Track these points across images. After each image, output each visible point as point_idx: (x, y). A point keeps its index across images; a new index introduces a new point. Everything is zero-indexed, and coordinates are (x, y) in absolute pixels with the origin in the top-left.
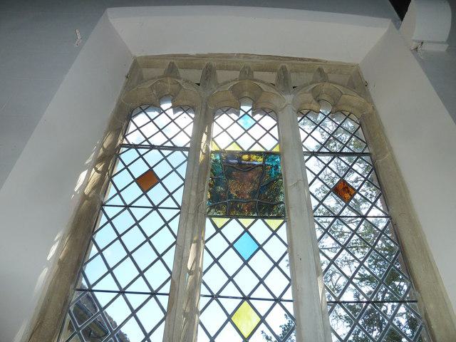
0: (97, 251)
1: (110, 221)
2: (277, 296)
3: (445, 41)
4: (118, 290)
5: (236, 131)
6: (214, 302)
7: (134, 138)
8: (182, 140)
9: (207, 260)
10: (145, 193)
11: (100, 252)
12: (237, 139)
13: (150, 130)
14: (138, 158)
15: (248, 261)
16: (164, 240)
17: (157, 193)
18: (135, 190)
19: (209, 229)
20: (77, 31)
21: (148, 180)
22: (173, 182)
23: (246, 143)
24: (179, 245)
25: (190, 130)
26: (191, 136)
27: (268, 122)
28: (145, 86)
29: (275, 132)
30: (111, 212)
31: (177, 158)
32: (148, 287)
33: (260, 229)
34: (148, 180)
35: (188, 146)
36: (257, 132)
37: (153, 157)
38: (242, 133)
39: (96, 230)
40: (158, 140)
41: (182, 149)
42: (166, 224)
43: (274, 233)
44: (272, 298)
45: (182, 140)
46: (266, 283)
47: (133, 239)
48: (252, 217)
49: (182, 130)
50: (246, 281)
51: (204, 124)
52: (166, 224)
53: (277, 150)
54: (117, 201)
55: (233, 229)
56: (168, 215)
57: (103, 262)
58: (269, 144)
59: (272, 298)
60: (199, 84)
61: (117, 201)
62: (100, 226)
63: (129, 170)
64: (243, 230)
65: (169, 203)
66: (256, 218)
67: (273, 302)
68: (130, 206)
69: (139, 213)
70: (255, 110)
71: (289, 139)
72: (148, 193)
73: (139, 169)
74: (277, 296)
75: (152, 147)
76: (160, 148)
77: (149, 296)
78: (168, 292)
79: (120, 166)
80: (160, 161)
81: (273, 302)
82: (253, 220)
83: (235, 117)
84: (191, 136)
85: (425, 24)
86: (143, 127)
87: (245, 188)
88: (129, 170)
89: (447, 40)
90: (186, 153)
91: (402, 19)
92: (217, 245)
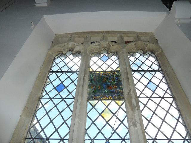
0: (37, 121)
1: (43, 106)
3: (190, 18)
4: (49, 140)
5: (100, 63)
7: (55, 69)
9: (69, 122)
10: (59, 93)
11: (139, 67)
12: (103, 63)
13: (61, 65)
14: (49, 92)
16: (67, 114)
17: (64, 93)
18: (55, 92)
19: (89, 107)
20: (32, 22)
21: (60, 88)
22: (72, 87)
23: (104, 67)
26: (79, 66)
27: (114, 58)
28: (60, 46)
29: (117, 62)
30: (43, 101)
33: (114, 105)
34: (60, 88)
35: (78, 70)
36: (109, 62)
37: (63, 77)
39: (36, 111)
40: (65, 69)
41: (76, 72)
42: (68, 106)
43: (120, 107)
46: (40, 123)
47: (53, 114)
49: (76, 64)
50: (107, 132)
54: (47, 97)
55: (100, 106)
57: (65, 135)
58: (115, 67)
59: (167, 138)
60: (82, 43)
61: (47, 97)
62: (39, 108)
64: (105, 107)
65: (70, 96)
68: (53, 98)
72: (60, 93)
73: (57, 83)
74: (123, 137)
75: (62, 72)
76: (65, 72)
78: (68, 138)
79: (54, 64)
83: (100, 57)
84: (79, 66)
85: (179, 10)
86: (59, 63)
87: (106, 86)
89: (190, 18)
90: (78, 73)
91: (170, 10)
92: (93, 115)
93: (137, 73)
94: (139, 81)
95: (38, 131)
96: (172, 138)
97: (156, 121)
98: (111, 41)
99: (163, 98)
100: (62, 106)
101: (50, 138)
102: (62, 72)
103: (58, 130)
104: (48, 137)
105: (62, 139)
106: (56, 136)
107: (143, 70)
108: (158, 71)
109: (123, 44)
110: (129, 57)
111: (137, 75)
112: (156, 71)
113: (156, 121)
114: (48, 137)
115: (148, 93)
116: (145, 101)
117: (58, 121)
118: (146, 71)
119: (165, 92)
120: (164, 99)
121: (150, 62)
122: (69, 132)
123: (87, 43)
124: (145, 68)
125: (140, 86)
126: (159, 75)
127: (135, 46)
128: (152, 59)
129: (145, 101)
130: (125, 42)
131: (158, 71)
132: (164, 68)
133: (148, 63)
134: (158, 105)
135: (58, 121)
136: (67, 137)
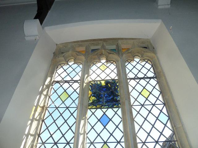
2: (157, 140)
5: (99, 72)
6: (119, 144)
8: (77, 78)
15: (103, 126)
16: (71, 121)
24: (78, 123)
25: (80, 74)
27: (113, 67)
28: (60, 55)
31: (76, 85)
32: (153, 139)
33: (110, 112)
36: (108, 71)
38: (103, 72)
44: (141, 142)
45: (77, 78)
47: (60, 122)
48: (106, 108)
50: (105, 135)
51: (86, 71)
52: (72, 114)
53: (117, 78)
55: (99, 113)
56: (72, 110)
58: (114, 76)
59: (141, 142)
63: (148, 71)
66: (108, 108)
67: (117, 143)
69: (61, 110)
70: (107, 61)
71: (121, 71)
74: (157, 140)
77: (70, 142)
80: (141, 69)
81: (155, 143)
82: (107, 109)
87: (107, 95)
88: (148, 71)
92: (93, 120)
93: (132, 81)
94: (154, 87)
95: (163, 144)
96: (159, 141)
97: (147, 126)
98: (144, 47)
99: (154, 105)
100: (67, 115)
101: (58, 142)
102: (66, 82)
103: (62, 135)
104: (68, 141)
105: (68, 143)
106: (50, 140)
107: (139, 78)
108: (153, 78)
109: (116, 50)
110: (126, 64)
111: (132, 83)
112: (150, 78)
113: (147, 126)
114: (68, 141)
115: (141, 100)
116: (138, 108)
117: (65, 128)
118: (140, 79)
119: (156, 99)
120: (155, 106)
121: (147, 69)
122: (73, 137)
123: (91, 51)
124: (140, 75)
125: (134, 94)
126: (153, 82)
127: (64, 58)
128: (148, 66)
129: (138, 108)
130: (92, 50)
131: (153, 78)
132: (158, 76)
133: (144, 71)
134: (150, 112)
135: (65, 128)
136: (72, 141)
